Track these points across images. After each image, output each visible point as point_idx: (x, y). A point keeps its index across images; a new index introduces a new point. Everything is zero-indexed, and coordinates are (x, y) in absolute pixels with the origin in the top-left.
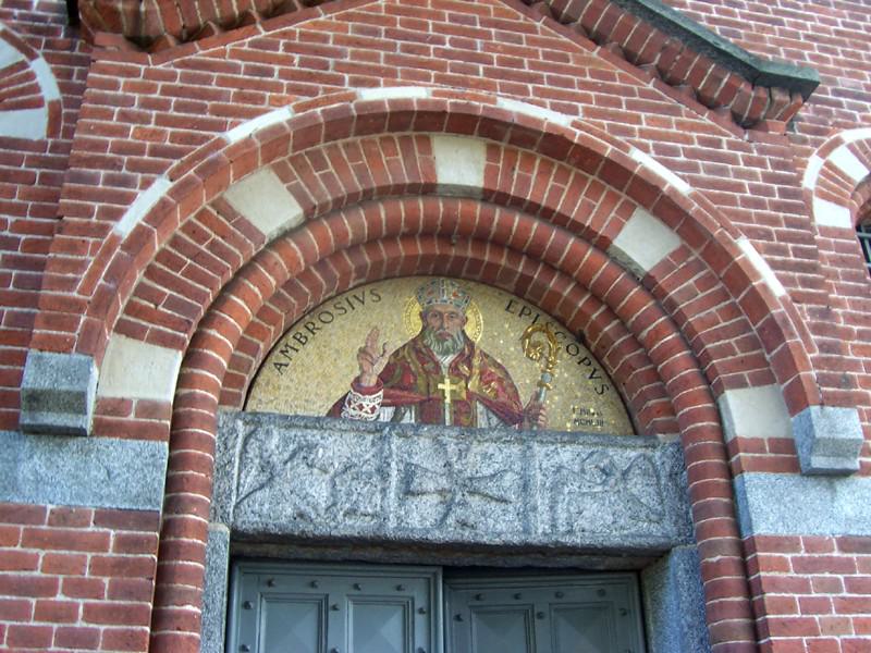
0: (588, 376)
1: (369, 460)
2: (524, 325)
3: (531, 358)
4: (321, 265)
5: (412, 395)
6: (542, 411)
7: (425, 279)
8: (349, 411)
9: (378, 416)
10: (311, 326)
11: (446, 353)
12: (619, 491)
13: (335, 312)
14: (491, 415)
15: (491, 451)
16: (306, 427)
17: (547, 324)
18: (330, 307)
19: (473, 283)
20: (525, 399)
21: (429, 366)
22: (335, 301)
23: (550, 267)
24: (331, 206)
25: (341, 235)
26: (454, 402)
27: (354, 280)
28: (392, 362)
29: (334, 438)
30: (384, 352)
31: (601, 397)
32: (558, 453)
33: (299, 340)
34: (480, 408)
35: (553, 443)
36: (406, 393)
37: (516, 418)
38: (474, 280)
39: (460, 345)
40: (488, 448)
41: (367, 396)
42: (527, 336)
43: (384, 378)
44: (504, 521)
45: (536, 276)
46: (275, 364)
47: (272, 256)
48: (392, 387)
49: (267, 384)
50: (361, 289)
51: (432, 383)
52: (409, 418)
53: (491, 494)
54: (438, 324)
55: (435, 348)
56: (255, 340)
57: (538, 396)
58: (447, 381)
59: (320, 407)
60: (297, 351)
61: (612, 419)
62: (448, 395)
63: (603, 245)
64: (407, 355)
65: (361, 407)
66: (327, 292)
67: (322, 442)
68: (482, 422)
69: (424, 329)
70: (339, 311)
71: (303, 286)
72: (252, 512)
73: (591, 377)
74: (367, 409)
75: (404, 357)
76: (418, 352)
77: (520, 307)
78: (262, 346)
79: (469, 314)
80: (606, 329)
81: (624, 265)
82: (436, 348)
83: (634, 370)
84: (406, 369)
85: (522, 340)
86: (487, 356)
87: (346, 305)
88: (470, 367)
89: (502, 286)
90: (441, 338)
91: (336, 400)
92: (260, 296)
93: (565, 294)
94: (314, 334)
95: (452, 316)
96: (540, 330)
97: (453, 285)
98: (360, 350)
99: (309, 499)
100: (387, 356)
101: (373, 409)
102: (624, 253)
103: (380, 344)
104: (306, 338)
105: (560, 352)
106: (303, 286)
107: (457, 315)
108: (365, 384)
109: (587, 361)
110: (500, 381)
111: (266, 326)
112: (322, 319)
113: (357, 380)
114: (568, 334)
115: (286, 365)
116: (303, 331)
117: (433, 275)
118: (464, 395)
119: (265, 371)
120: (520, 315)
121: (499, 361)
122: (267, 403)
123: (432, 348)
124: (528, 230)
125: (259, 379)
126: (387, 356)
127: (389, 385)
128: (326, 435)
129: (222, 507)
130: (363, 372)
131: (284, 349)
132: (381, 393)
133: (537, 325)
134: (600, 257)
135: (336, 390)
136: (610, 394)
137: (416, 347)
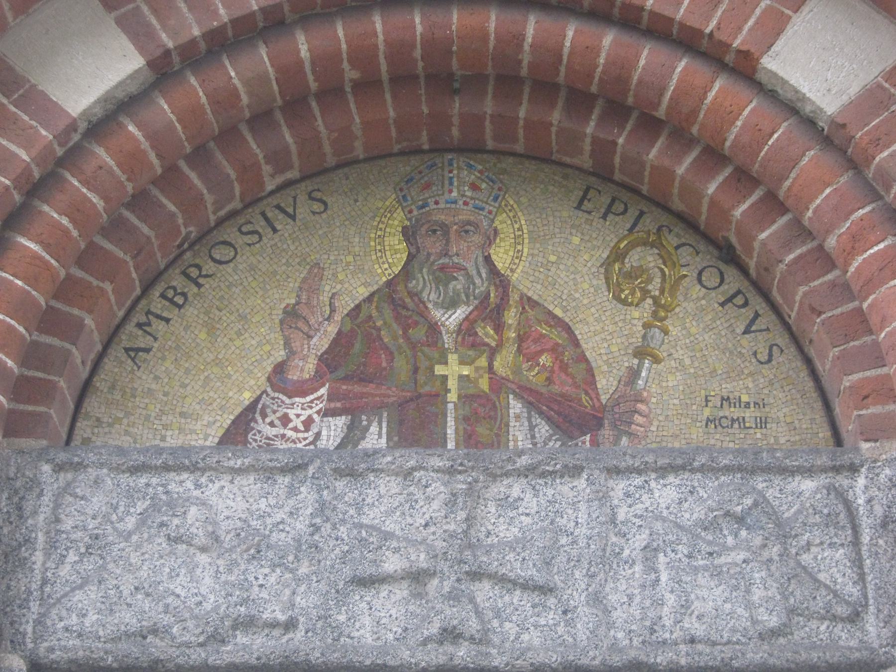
0: (740, 329)
1: (282, 522)
2: (608, 234)
3: (624, 302)
4: (199, 156)
5: (383, 390)
6: (641, 407)
7: (415, 161)
8: (264, 428)
9: (318, 435)
10: (194, 272)
11: (452, 304)
12: (770, 560)
13: (240, 240)
14: (537, 420)
15: (516, 492)
16: (167, 468)
17: (659, 229)
18: (230, 233)
19: (511, 160)
20: (606, 385)
21: (419, 333)
22: (241, 220)
23: (650, 125)
24: (203, 46)
25: (225, 100)
26: (465, 398)
27: (272, 176)
28: (348, 327)
29: (217, 485)
30: (333, 311)
31: (765, 370)
32: (651, 491)
33: (171, 301)
34: (516, 406)
35: (639, 472)
36: (370, 388)
37: (580, 416)
38: (513, 154)
39: (481, 285)
40: (510, 486)
41: (297, 399)
42: (618, 255)
43: (329, 362)
44: (536, 627)
45: (621, 141)
46: (127, 350)
47: (93, 153)
48: (346, 379)
49: (113, 387)
50: (291, 192)
51: (423, 364)
52: (376, 437)
53: (512, 575)
54: (438, 247)
55: (430, 295)
56: (76, 312)
57: (634, 374)
58: (453, 358)
59: (209, 425)
60: (167, 320)
61: (790, 418)
62: (452, 384)
63: (744, 69)
64: (375, 313)
65: (285, 420)
66: (218, 206)
67: (197, 493)
68: (518, 435)
69: (411, 257)
70: (248, 239)
71: (165, 201)
72: (67, 629)
73: (747, 331)
74: (298, 423)
75: (370, 317)
76: (397, 305)
77: (606, 200)
78: (89, 321)
79: (502, 222)
80: (763, 236)
81: (789, 105)
82: (433, 296)
83: (820, 314)
84: (373, 340)
85: (607, 264)
86: (533, 304)
87: (260, 225)
88: (499, 328)
89: (567, 160)
90: (444, 275)
91: (239, 410)
92: (75, 233)
93: (681, 170)
94: (199, 286)
95: (466, 228)
96: (645, 244)
97: (470, 167)
98: (285, 312)
99: (170, 600)
100: (338, 317)
101: (308, 423)
102: (784, 82)
103: (325, 298)
104: (184, 294)
105: (685, 283)
106: (165, 201)
107: (477, 226)
108: (293, 376)
109: (739, 300)
110: (555, 350)
111: (95, 283)
112: (218, 257)
113: (280, 369)
114: (702, 247)
115: (147, 350)
116: (178, 282)
117: (431, 151)
118: (484, 384)
119: (108, 364)
120: (604, 217)
121: (558, 312)
122: (110, 425)
123: (425, 295)
124: (595, 51)
125: (97, 382)
126: (338, 317)
127: (341, 373)
128: (203, 480)
129: (12, 624)
130: (291, 353)
131: (143, 319)
132: (323, 391)
133: (638, 234)
134: (741, 90)
135: (240, 391)
136: (788, 361)
137: (394, 295)
